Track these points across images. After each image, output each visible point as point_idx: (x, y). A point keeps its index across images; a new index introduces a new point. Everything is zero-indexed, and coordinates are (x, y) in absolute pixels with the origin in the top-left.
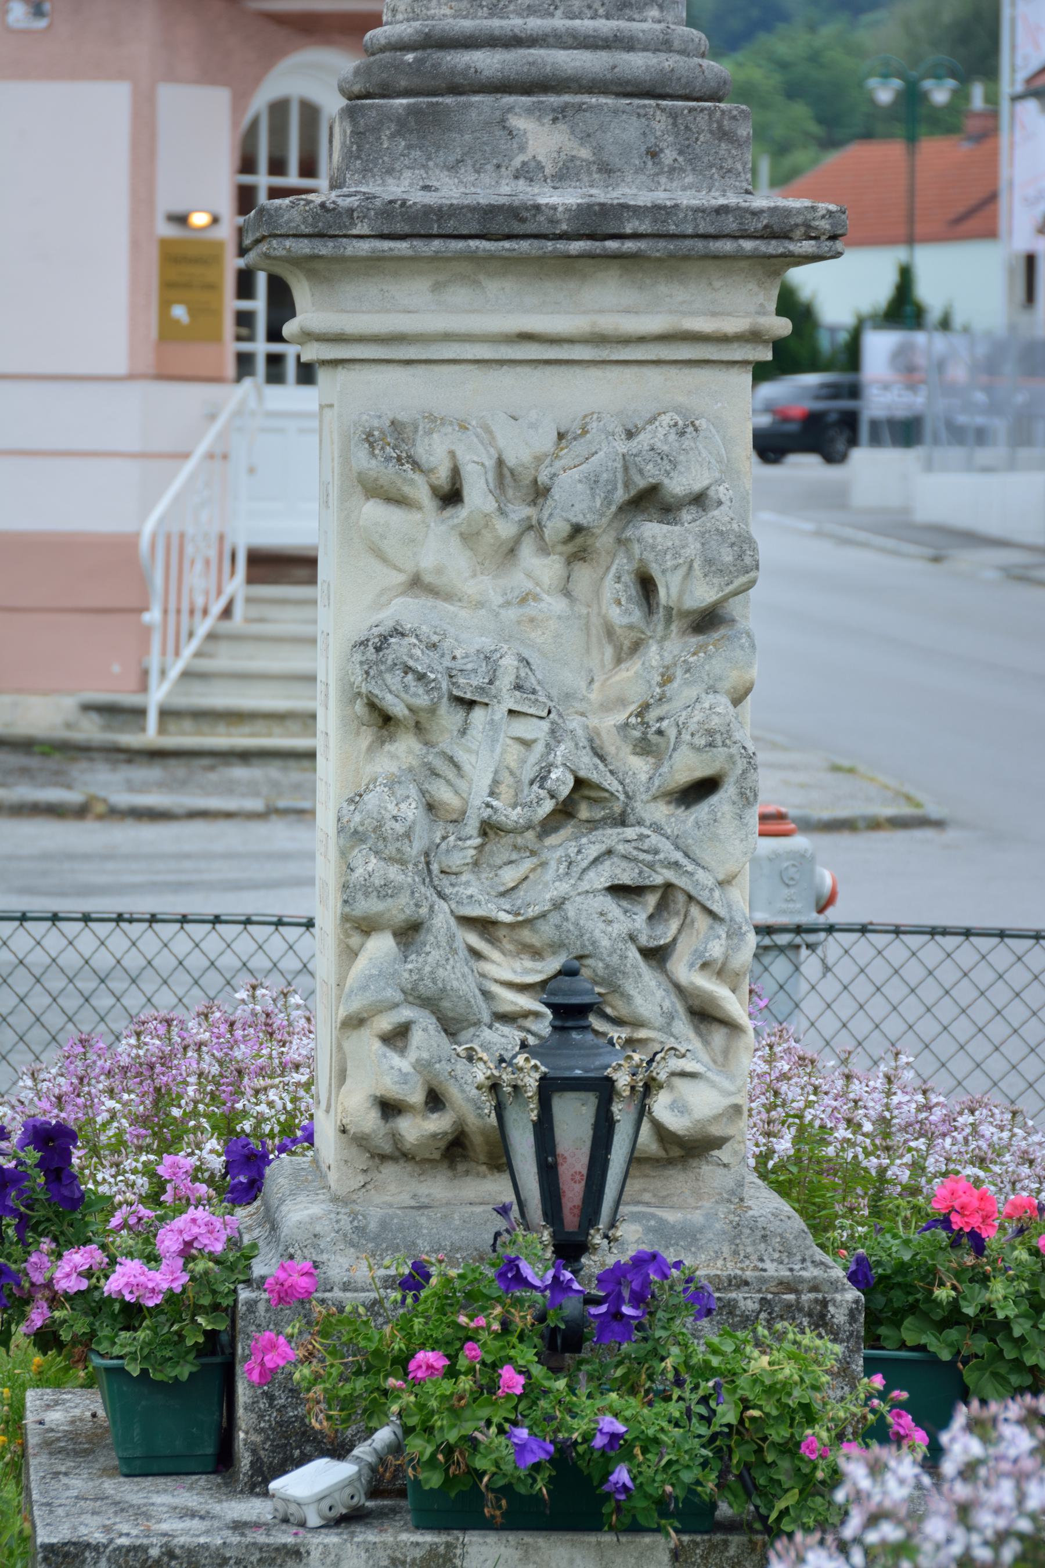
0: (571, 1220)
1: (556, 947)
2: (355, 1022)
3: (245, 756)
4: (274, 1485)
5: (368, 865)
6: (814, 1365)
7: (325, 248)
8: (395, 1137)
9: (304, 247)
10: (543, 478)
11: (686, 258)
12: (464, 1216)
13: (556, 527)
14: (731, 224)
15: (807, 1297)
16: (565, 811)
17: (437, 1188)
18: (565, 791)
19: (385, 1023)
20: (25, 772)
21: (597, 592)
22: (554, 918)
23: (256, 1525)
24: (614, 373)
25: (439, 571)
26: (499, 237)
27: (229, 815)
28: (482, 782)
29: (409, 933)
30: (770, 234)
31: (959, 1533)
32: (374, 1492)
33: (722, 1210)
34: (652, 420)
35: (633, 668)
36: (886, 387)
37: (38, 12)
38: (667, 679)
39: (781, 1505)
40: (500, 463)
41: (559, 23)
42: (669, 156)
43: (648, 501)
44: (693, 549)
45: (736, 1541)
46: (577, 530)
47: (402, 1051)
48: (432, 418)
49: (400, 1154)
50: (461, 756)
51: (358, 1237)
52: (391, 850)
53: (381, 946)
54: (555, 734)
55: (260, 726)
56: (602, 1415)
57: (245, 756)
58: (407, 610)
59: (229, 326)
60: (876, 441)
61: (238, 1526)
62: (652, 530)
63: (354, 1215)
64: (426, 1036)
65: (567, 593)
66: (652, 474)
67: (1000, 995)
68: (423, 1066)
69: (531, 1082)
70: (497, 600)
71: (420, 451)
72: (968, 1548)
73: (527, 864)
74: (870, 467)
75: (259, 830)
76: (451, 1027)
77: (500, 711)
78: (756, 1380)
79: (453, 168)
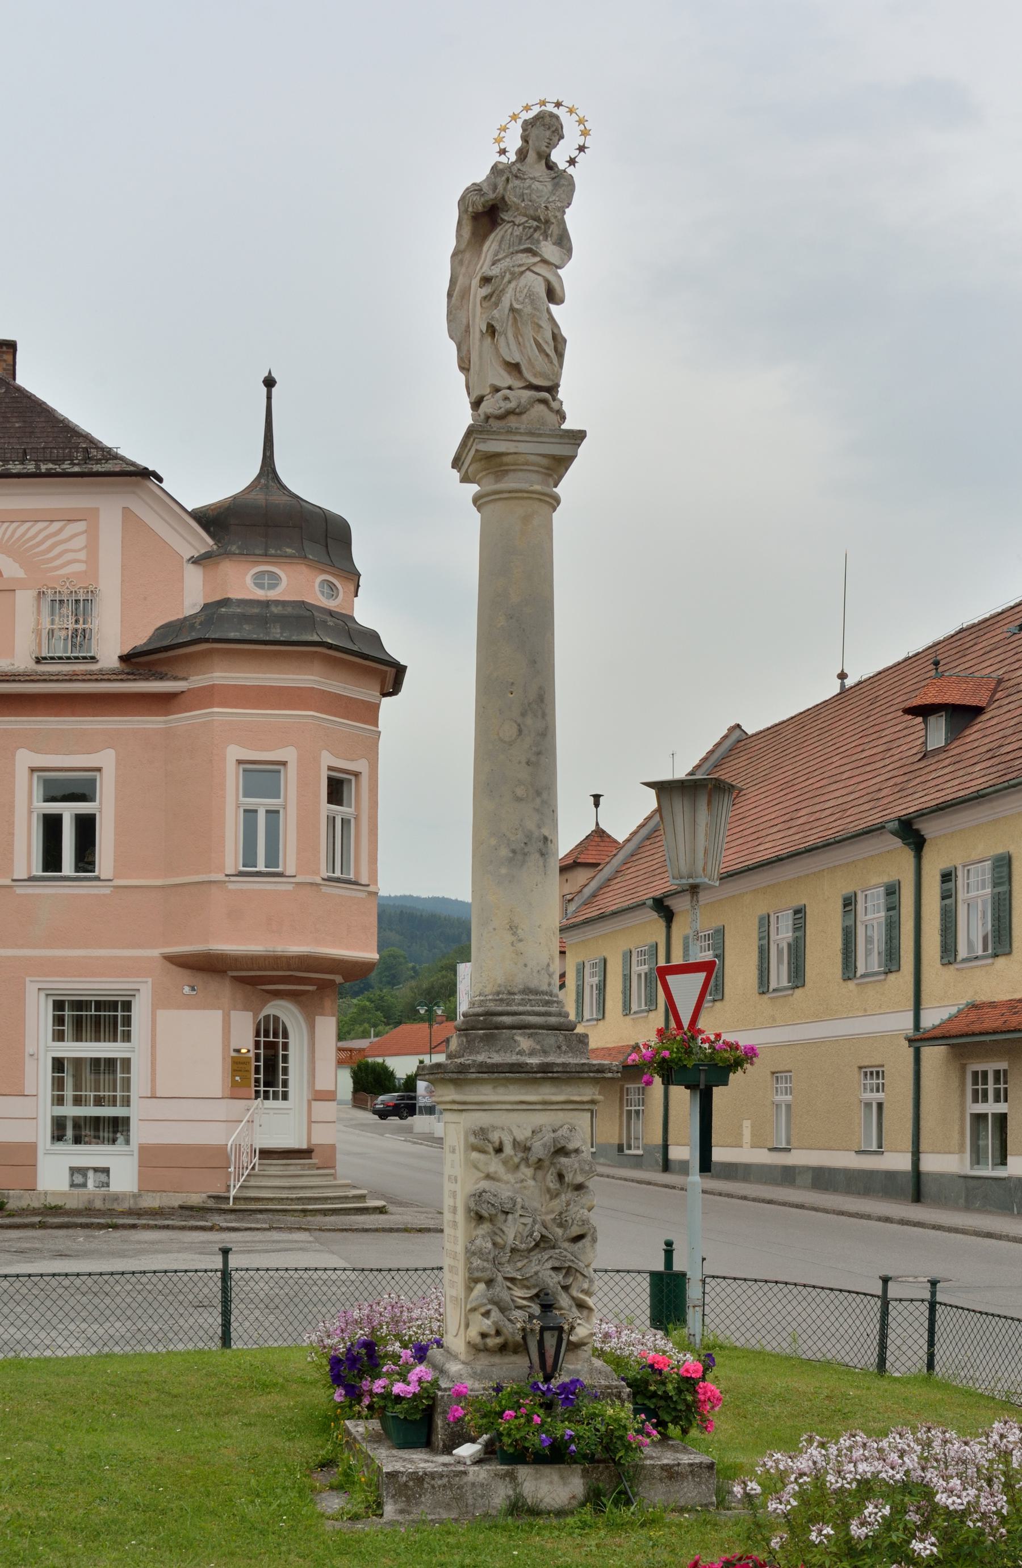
0: (549, 1370)
1: (535, 1286)
2: (473, 1310)
3: (261, 1211)
4: (454, 1452)
5: (477, 1262)
6: (622, 1412)
7: (461, 1076)
8: (485, 1344)
9: (455, 1076)
10: (528, 1144)
11: (572, 1078)
12: (514, 1369)
13: (533, 1159)
14: (586, 1068)
15: (615, 1391)
16: (537, 1245)
17: (496, 1359)
18: (538, 1239)
19: (483, 1310)
20: (192, 1216)
21: (544, 1179)
22: (535, 1277)
23: (450, 1464)
24: (548, 1113)
25: (496, 1173)
26: (516, 1073)
27: (258, 1229)
28: (511, 1236)
29: (490, 1283)
30: (598, 1071)
31: (840, 1480)
32: (486, 1453)
33: (586, 1365)
34: (561, 1127)
35: (555, 1202)
36: (424, 1097)
37: (193, 989)
38: (568, 1205)
39: (620, 1455)
40: (514, 1140)
41: (528, 1008)
42: (564, 1048)
43: (561, 1151)
44: (576, 1165)
45: (601, 1465)
46: (540, 1160)
47: (488, 1318)
48: (493, 1127)
49: (486, 1349)
50: (505, 1229)
51: (474, 1375)
52: (485, 1257)
53: (481, 1287)
54: (534, 1222)
55: (265, 1202)
56: (566, 1430)
57: (261, 1211)
58: (484, 1184)
59: (253, 1083)
60: (421, 1113)
61: (444, 1465)
62: (563, 1160)
63: (472, 1368)
64: (495, 1314)
65: (534, 1179)
66: (563, 1143)
67: (611, 1295)
68: (495, 1323)
69: (538, 1328)
70: (513, 1181)
71: (490, 1136)
72: (843, 1485)
73: (526, 1261)
74: (419, 1122)
75: (269, 1233)
76: (503, 1310)
77: (517, 1215)
78: (610, 1417)
79: (497, 1052)
